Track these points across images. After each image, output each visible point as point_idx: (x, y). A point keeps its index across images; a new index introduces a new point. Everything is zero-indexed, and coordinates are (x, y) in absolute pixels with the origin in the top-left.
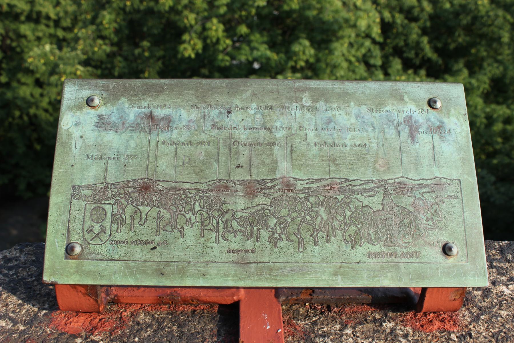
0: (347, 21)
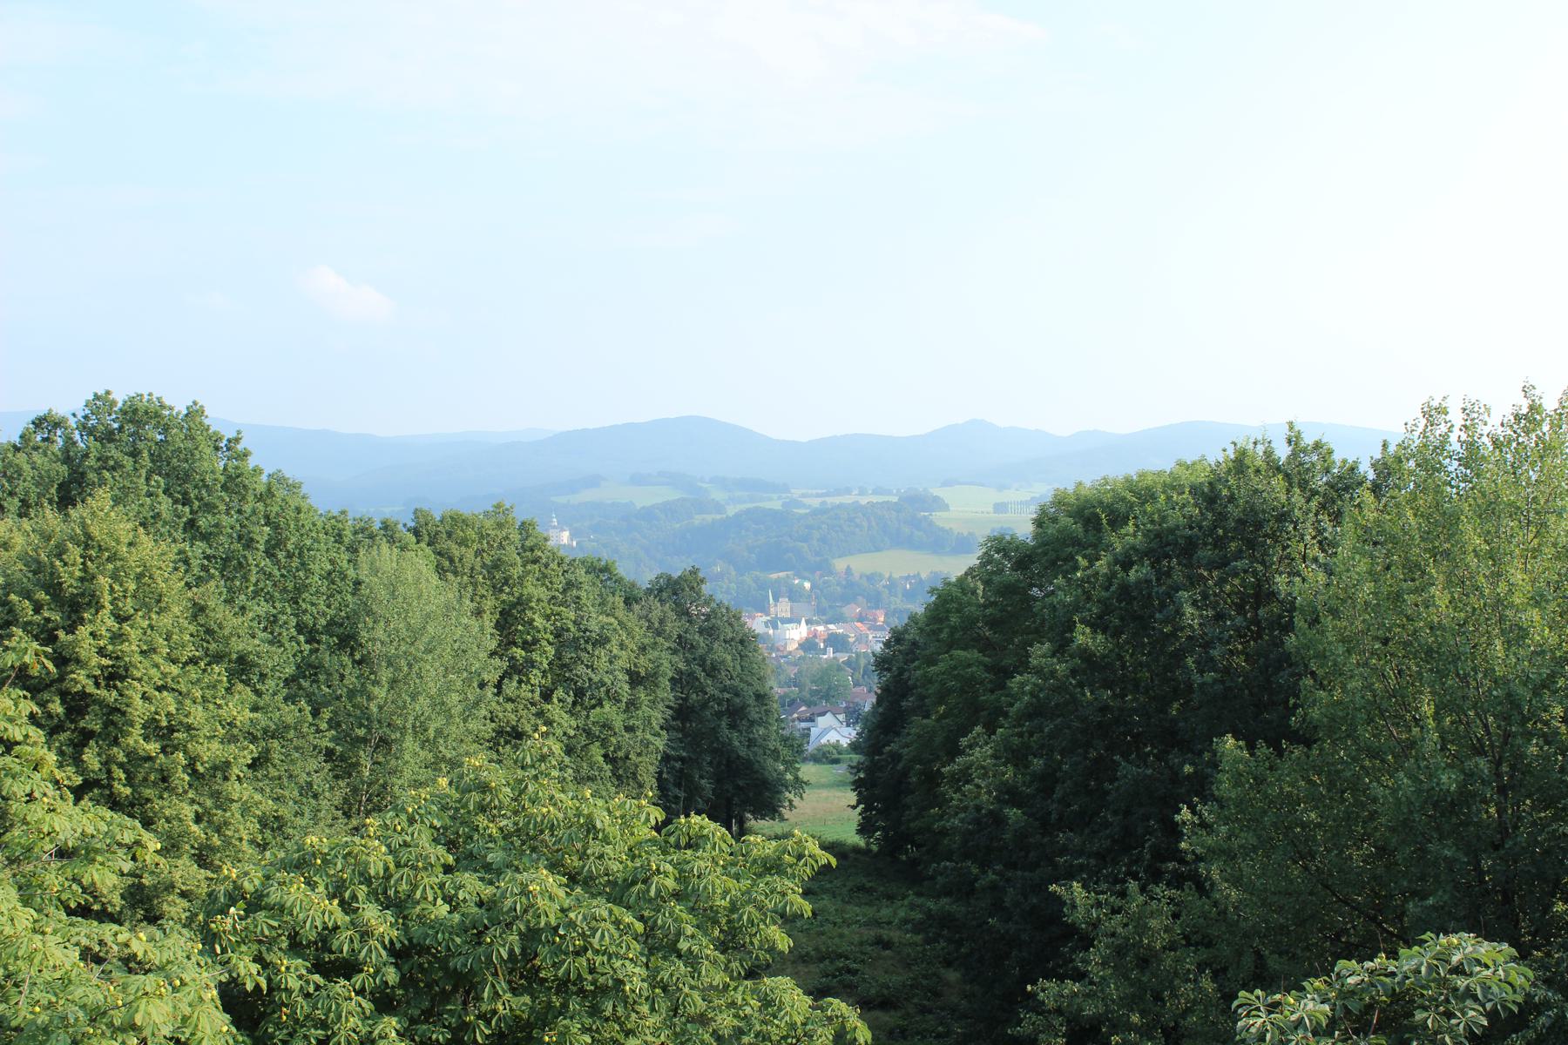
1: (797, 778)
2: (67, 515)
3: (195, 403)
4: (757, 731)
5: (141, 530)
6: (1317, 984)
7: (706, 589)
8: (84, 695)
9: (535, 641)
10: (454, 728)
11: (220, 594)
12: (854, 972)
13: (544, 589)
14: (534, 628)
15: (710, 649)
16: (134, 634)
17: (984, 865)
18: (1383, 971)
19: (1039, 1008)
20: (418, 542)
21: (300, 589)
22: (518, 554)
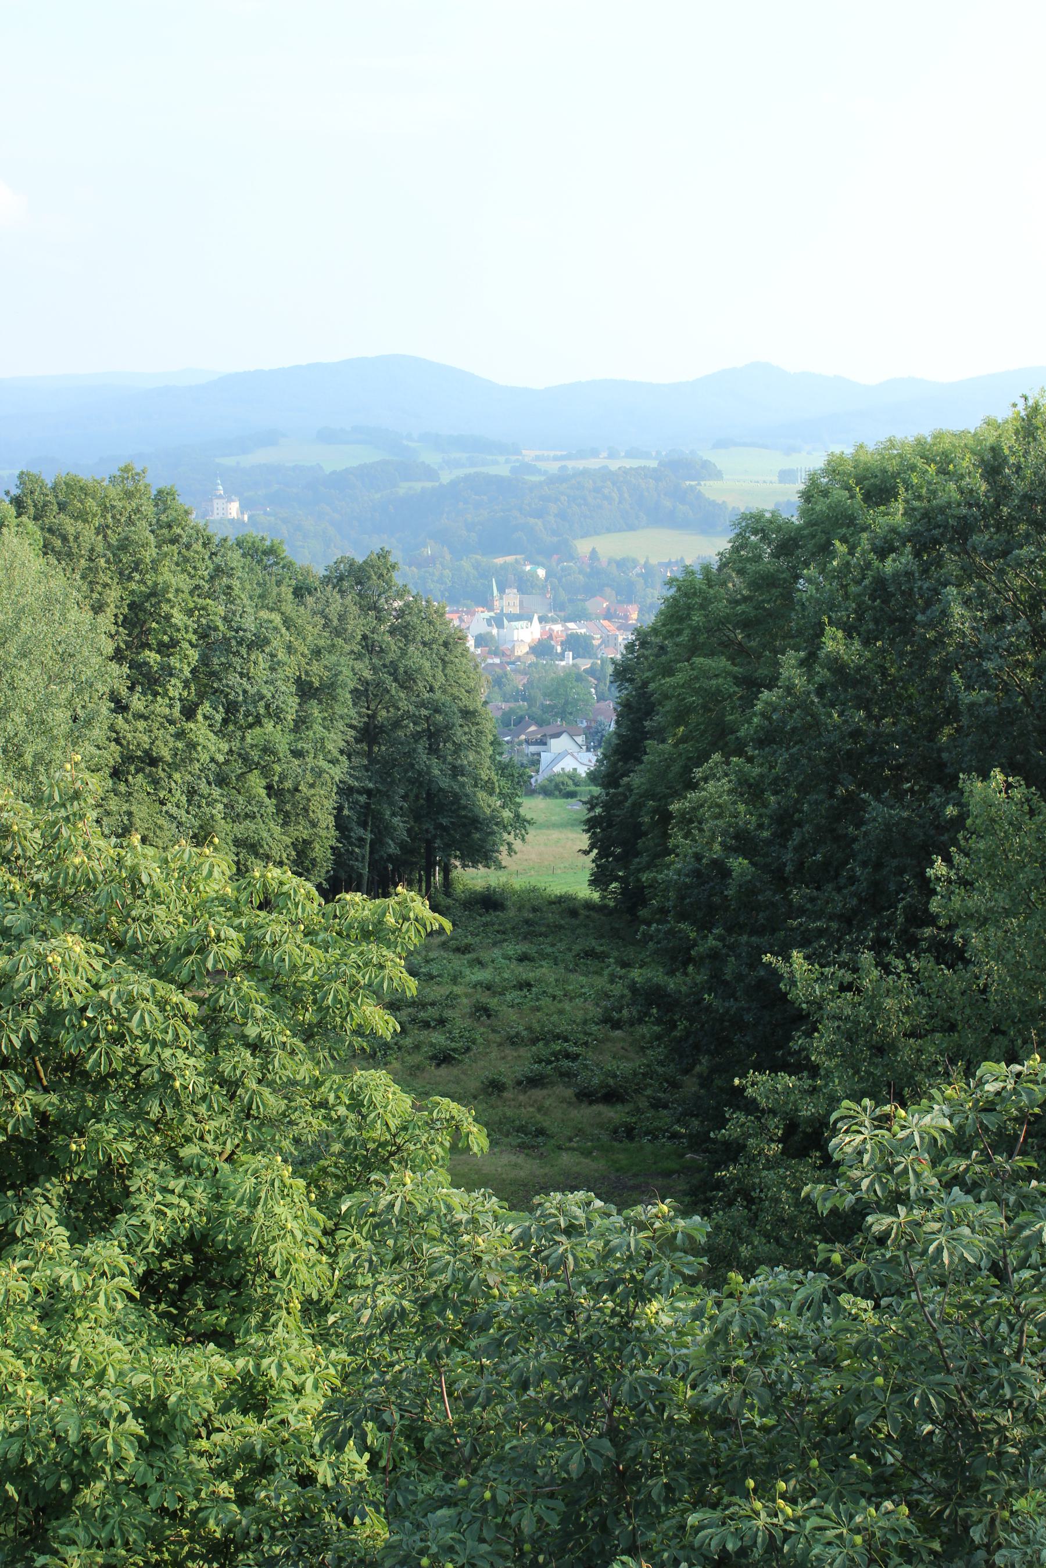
1: (517, 816)
4: (466, 757)
6: (949, 1092)
7: (398, 579)
9: (174, 643)
12: (574, 1057)
13: (185, 576)
14: (171, 626)
15: (404, 653)
17: (704, 926)
18: (1032, 1077)
19: (751, 1107)
20: (19, 515)
22: (152, 531)
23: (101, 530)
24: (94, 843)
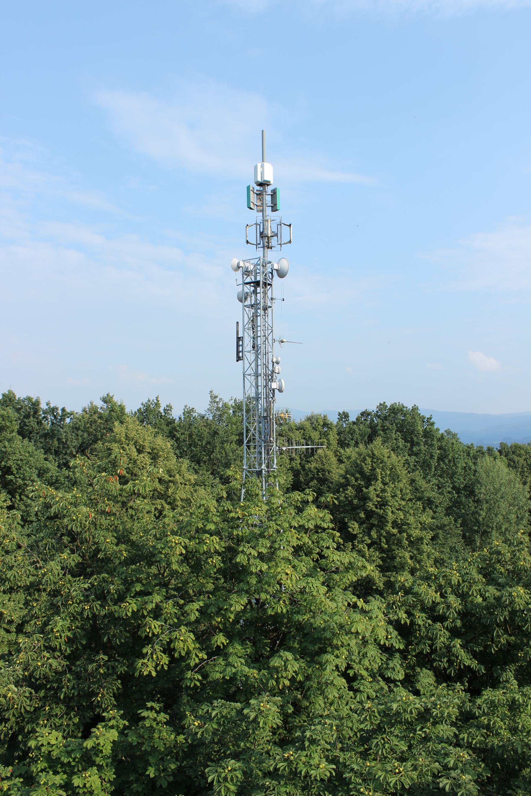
0: (341, 627)
2: (367, 447)
3: (415, 405)
5: (392, 452)
8: (371, 511)
10: (512, 528)
11: (421, 475)
16: (389, 490)
20: (501, 455)
21: (454, 473)
23: (525, 460)
24: (527, 558)
